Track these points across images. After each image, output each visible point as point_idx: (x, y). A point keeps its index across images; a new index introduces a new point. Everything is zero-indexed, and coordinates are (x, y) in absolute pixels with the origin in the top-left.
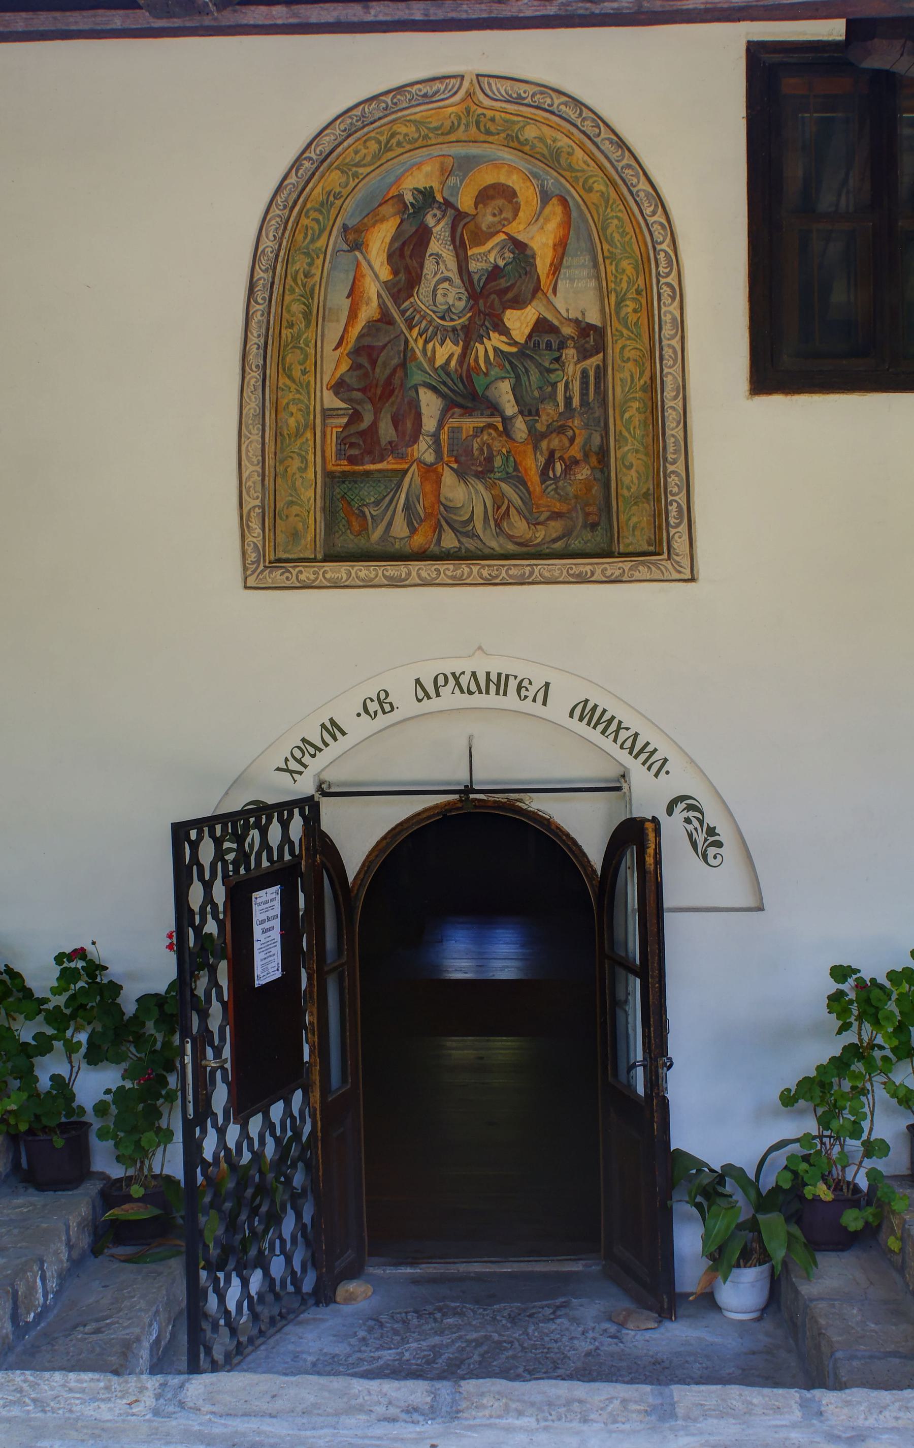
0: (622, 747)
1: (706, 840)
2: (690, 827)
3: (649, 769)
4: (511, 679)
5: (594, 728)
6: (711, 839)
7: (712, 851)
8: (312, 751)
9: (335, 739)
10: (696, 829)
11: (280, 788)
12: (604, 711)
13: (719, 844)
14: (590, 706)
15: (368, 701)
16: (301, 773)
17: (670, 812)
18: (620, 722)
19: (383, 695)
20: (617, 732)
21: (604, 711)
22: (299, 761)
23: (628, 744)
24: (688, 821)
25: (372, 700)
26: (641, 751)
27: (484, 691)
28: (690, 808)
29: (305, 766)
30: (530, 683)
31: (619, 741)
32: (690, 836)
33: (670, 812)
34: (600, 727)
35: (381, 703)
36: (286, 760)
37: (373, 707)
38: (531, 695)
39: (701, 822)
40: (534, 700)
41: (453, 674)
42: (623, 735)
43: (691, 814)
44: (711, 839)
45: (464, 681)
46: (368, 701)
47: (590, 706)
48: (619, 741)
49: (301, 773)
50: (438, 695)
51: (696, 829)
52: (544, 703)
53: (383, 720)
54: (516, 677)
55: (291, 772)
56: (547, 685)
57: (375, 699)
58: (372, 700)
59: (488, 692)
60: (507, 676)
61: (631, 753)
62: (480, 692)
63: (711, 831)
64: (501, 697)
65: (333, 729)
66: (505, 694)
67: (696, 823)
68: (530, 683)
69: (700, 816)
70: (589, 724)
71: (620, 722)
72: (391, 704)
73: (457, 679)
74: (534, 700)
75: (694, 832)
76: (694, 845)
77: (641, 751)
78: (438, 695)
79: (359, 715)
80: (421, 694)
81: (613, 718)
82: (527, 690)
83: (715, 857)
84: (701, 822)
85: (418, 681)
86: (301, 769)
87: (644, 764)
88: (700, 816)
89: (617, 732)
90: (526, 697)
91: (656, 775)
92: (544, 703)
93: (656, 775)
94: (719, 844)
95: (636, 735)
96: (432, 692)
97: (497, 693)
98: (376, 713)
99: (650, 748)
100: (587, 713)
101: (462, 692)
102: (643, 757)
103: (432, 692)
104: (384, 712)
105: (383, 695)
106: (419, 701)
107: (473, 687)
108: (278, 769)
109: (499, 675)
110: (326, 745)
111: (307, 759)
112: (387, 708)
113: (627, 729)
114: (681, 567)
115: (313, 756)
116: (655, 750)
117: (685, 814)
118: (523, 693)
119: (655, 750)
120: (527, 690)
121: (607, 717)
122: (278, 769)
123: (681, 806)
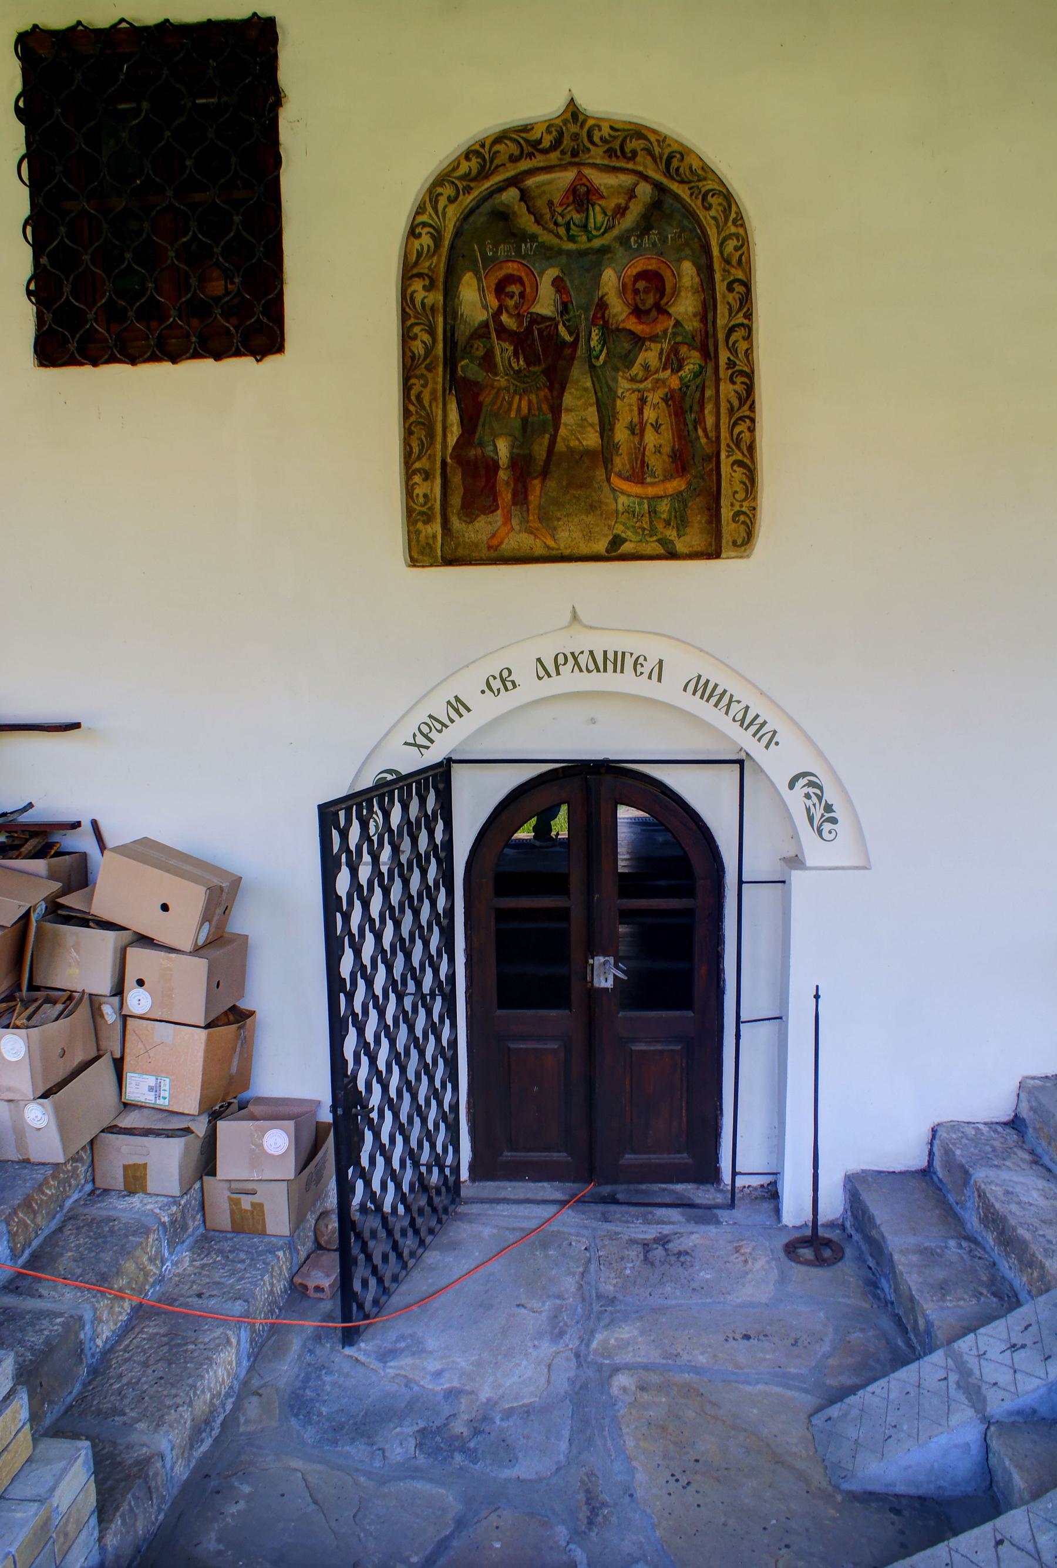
0: (734, 720)
1: (823, 815)
2: (809, 803)
3: (759, 740)
4: (627, 656)
5: (707, 701)
6: (827, 815)
7: (827, 827)
8: (439, 726)
9: (461, 716)
10: (814, 805)
11: (409, 762)
12: (716, 686)
13: (834, 821)
14: (702, 681)
15: (491, 679)
16: (427, 748)
17: (792, 785)
18: (732, 696)
19: (505, 674)
20: (729, 705)
21: (716, 686)
22: (426, 736)
23: (739, 717)
24: (808, 796)
25: (495, 678)
26: (751, 724)
27: (602, 669)
28: (811, 784)
29: (432, 741)
30: (645, 659)
31: (584, 669)
32: (808, 810)
33: (792, 785)
34: (714, 700)
35: (503, 681)
36: (414, 735)
37: (496, 684)
38: (646, 670)
39: (820, 798)
40: (650, 677)
41: (573, 654)
42: (735, 708)
43: (811, 790)
44: (827, 815)
45: (583, 660)
46: (491, 679)
47: (702, 681)
48: (584, 669)
49: (427, 748)
50: (558, 674)
51: (814, 805)
52: (659, 680)
53: (508, 700)
54: (632, 654)
55: (419, 746)
56: (661, 662)
57: (498, 676)
58: (495, 678)
59: (605, 670)
60: (623, 654)
61: (741, 725)
62: (598, 671)
63: (829, 808)
64: (618, 674)
65: (458, 706)
66: (622, 671)
67: (815, 799)
68: (645, 659)
69: (818, 792)
70: (702, 697)
71: (732, 696)
72: (513, 682)
73: (575, 659)
74: (650, 677)
75: (812, 808)
76: (811, 819)
77: (751, 724)
78: (558, 674)
79: (483, 692)
80: (542, 673)
81: (725, 691)
82: (642, 666)
83: (830, 832)
84: (820, 798)
85: (539, 660)
86: (428, 744)
87: (754, 735)
88: (818, 792)
89: (729, 705)
90: (642, 673)
91: (767, 747)
92: (659, 680)
93: (767, 747)
94: (834, 821)
95: (747, 708)
96: (552, 670)
97: (615, 671)
98: (499, 690)
99: (759, 721)
100: (702, 688)
101: (581, 671)
102: (753, 729)
103: (552, 670)
104: (507, 690)
105: (505, 674)
106: (540, 678)
107: (591, 666)
108: (406, 744)
109: (616, 653)
110: (452, 721)
111: (433, 735)
112: (509, 685)
113: (739, 702)
114: (745, 484)
115: (440, 731)
116: (765, 723)
117: (806, 790)
118: (639, 669)
119: (765, 723)
120: (642, 666)
121: (719, 691)
122: (406, 744)
123: (802, 782)
